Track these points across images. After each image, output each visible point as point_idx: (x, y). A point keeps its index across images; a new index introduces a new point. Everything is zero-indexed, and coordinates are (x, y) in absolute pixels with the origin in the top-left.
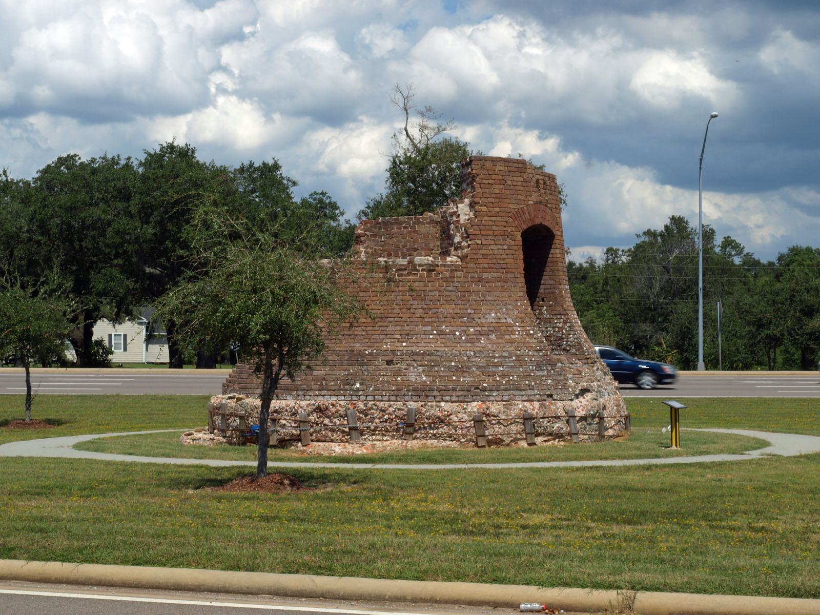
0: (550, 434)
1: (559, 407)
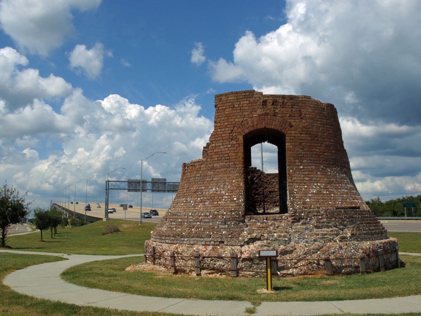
0: (213, 269)
1: (227, 251)
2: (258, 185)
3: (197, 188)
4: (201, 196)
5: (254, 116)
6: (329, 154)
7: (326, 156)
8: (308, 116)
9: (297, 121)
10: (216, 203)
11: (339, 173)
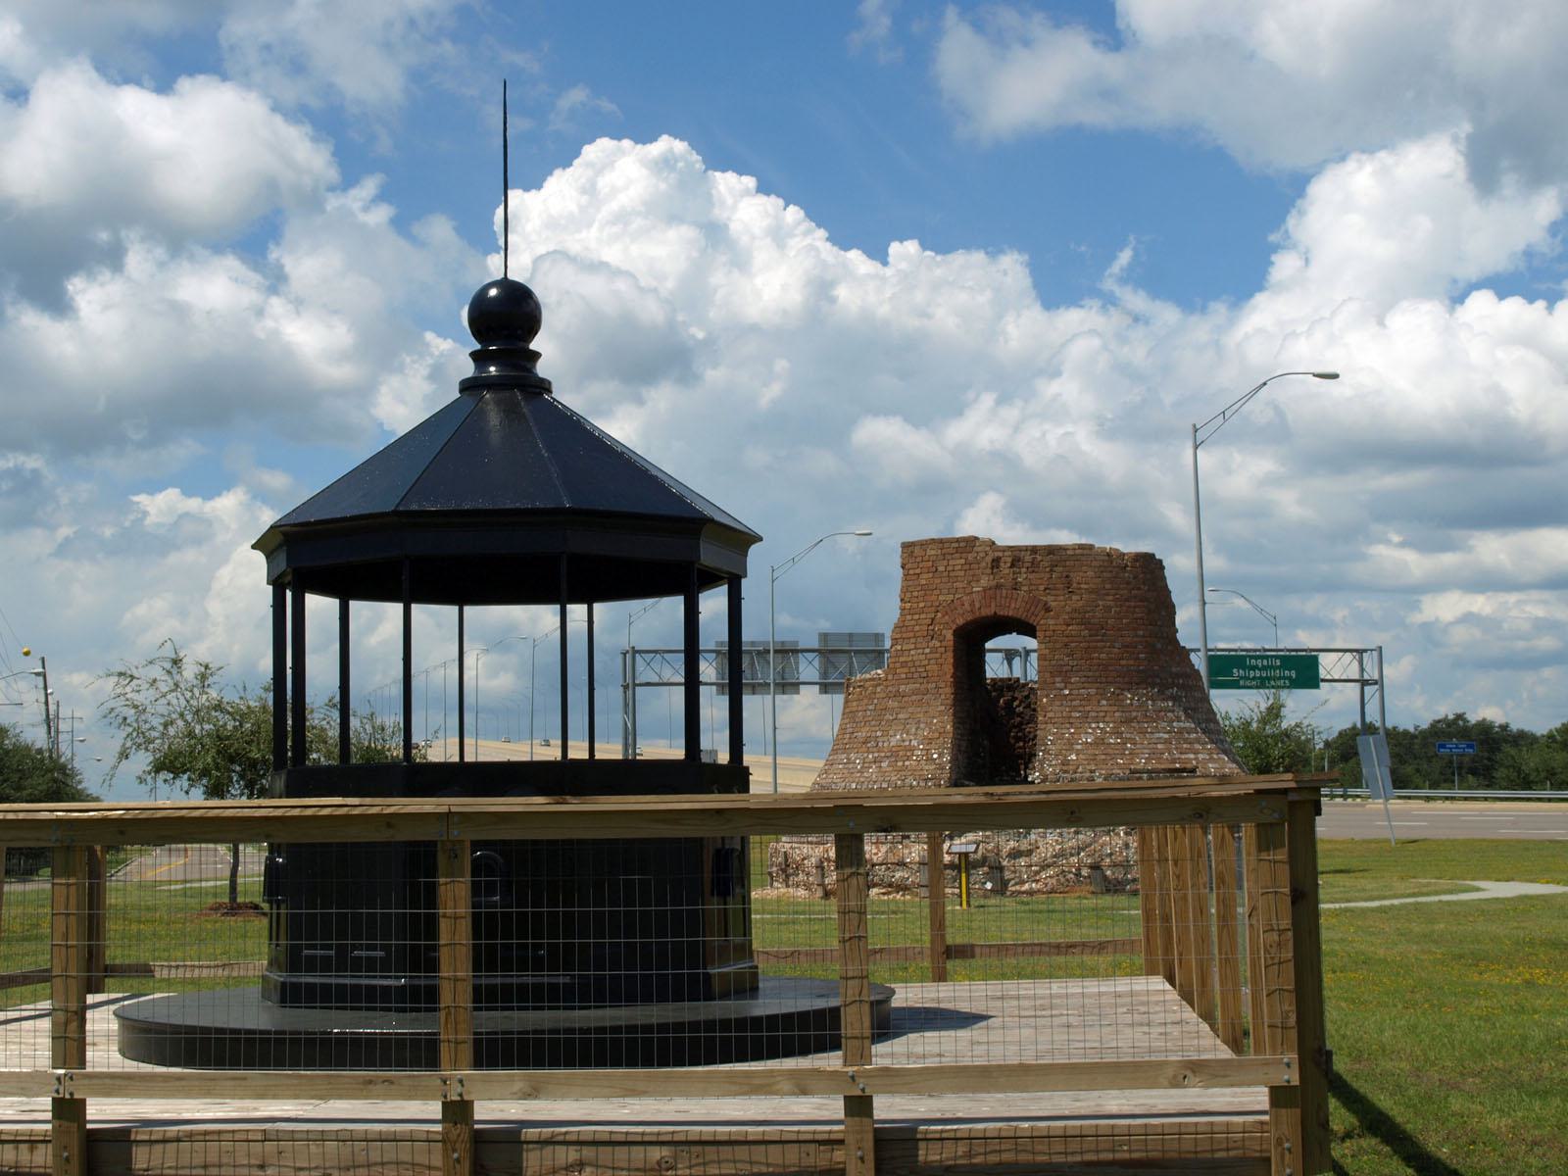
0: (890, 886)
2: (1023, 718)
3: (868, 735)
4: (875, 749)
5: (974, 589)
6: (1131, 662)
7: (1123, 666)
8: (1086, 586)
9: (1062, 598)
10: (900, 764)
11: (1153, 700)
